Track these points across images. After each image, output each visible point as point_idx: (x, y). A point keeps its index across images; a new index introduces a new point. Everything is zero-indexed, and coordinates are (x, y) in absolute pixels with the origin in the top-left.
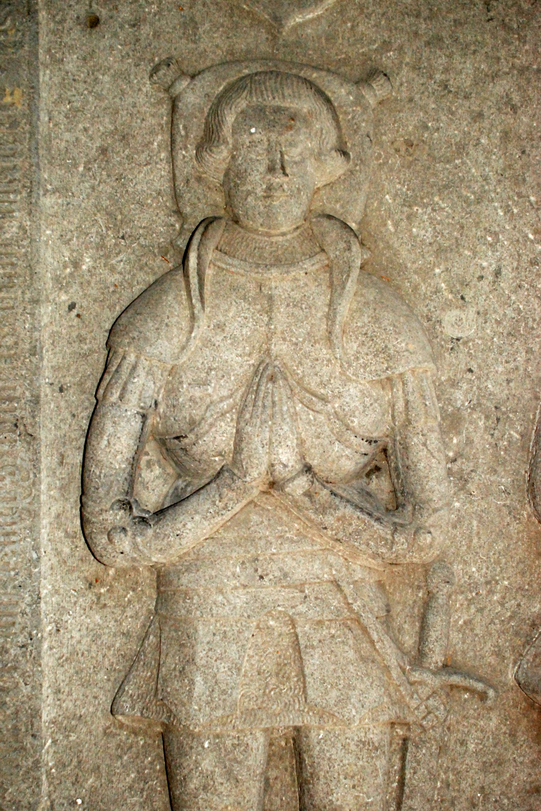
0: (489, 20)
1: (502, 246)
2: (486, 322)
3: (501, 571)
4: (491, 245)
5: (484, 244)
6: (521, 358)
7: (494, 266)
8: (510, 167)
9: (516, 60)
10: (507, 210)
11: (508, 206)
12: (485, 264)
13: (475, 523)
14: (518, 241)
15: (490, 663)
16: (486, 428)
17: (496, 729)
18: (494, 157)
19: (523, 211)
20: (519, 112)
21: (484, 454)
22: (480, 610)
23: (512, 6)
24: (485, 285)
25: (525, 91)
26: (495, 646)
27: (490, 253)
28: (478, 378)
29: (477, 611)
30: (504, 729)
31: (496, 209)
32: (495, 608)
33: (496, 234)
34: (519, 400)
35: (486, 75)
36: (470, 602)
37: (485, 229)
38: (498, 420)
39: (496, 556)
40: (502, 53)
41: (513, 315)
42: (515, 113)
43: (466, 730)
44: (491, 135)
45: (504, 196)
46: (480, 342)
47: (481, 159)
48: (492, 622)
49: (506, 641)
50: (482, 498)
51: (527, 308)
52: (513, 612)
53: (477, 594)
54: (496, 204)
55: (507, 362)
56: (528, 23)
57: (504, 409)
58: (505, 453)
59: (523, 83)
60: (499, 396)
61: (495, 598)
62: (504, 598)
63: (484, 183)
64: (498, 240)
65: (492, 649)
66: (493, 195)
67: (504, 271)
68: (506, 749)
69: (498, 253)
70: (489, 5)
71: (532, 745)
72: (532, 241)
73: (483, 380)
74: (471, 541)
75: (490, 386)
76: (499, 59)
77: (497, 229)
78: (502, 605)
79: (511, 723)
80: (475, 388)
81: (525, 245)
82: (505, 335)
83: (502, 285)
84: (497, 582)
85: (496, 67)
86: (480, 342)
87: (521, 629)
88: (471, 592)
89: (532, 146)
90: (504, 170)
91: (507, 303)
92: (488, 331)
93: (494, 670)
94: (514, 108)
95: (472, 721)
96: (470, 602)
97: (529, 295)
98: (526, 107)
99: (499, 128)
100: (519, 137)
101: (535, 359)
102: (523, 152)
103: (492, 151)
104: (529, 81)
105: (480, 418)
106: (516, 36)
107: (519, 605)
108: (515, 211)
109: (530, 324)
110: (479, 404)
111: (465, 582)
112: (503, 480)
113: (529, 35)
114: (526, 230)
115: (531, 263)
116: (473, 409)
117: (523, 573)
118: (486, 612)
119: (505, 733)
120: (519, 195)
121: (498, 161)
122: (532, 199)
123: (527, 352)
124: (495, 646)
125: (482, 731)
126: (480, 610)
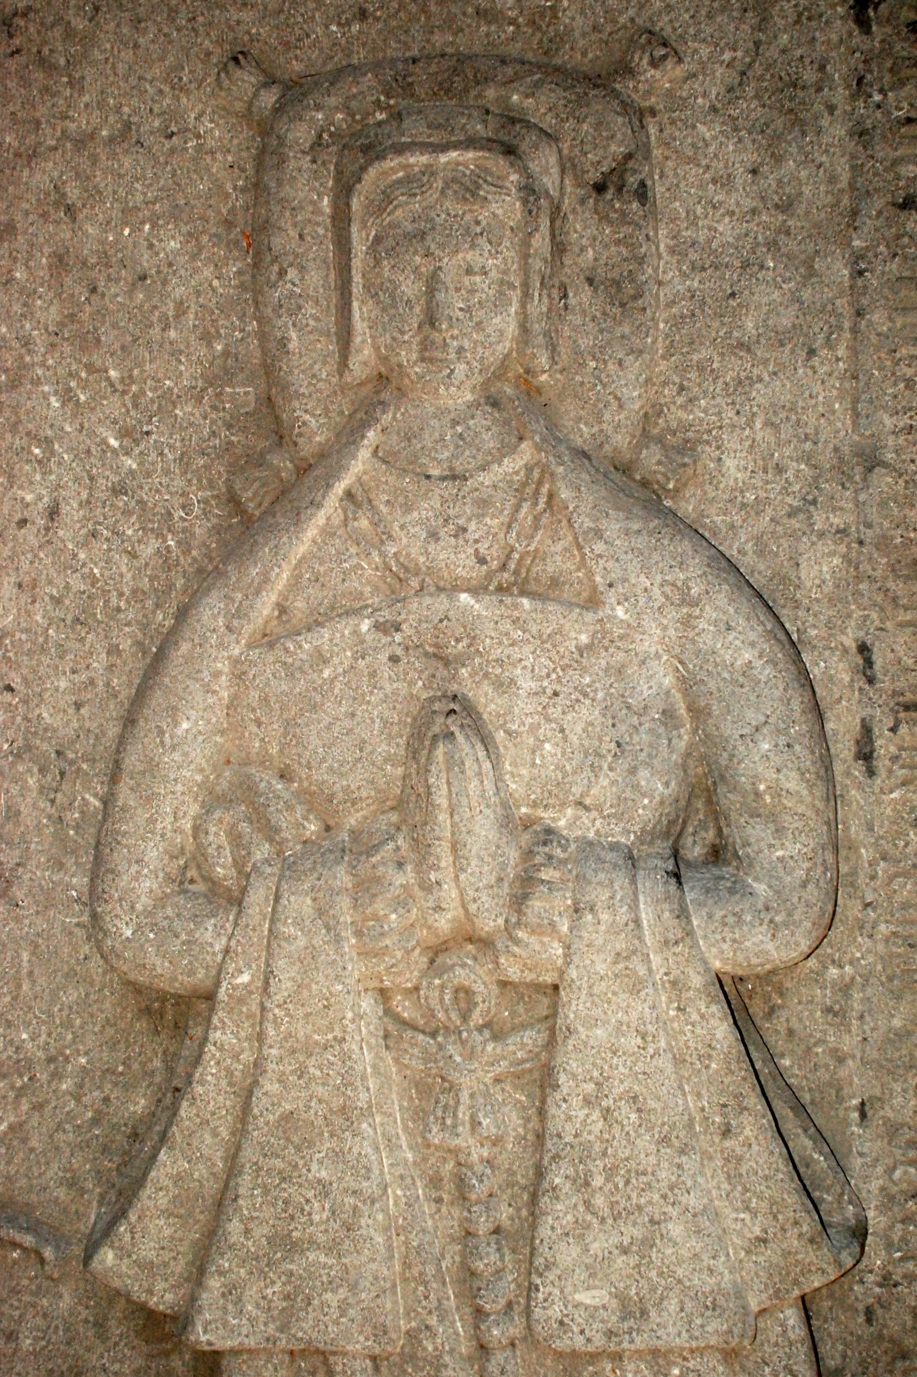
0: (12, 54)
1: (60, 463)
2: (34, 602)
3: (74, 1041)
4: (40, 462)
5: (28, 461)
6: (100, 661)
7: (46, 499)
8: (72, 317)
9: (67, 123)
10: (67, 397)
11: (70, 390)
12: (29, 498)
13: (25, 956)
14: (88, 452)
15: (57, 1198)
16: (42, 787)
17: (71, 1315)
18: (39, 302)
19: (96, 398)
20: (81, 216)
21: (40, 835)
22: (38, 1107)
23: (53, 25)
24: (30, 535)
25: (88, 178)
26: (65, 1170)
27: (38, 477)
28: (25, 702)
29: (34, 1108)
30: (85, 1313)
31: (45, 397)
32: (65, 1105)
33: (48, 441)
34: (97, 738)
35: (18, 155)
36: (21, 1092)
37: (28, 434)
38: (62, 774)
39: (65, 1013)
40: (42, 112)
41: (82, 588)
42: (74, 220)
43: (17, 1313)
44: (32, 264)
45: (61, 371)
46: (24, 637)
47: (17, 308)
48: (59, 1127)
49: (86, 1161)
50: (38, 913)
51: (107, 573)
52: (98, 1112)
53: (30, 1079)
54: (46, 388)
55: (74, 672)
56: (85, 55)
57: (71, 756)
58: (77, 833)
59: (84, 164)
60: (62, 732)
61: (64, 1087)
62: (81, 1086)
63: (23, 351)
64: (53, 453)
65: (61, 1174)
66: (40, 372)
67: (64, 509)
68: (88, 1349)
69: (53, 477)
70: (10, 26)
71: (135, 1343)
72: (114, 451)
73: (32, 705)
74: (19, 986)
75: (45, 715)
76: (38, 123)
77: (49, 433)
78: (78, 1099)
79: (98, 1304)
80: (19, 719)
81: (101, 459)
82: (68, 622)
83: (61, 533)
84: (67, 1059)
85: (31, 139)
86: (24, 637)
87: (113, 1142)
88: (21, 1076)
89: (109, 279)
90: (61, 324)
91: (70, 565)
92: (38, 618)
93: (65, 1211)
94: (70, 210)
95: (27, 1298)
96: (21, 1092)
97: (110, 550)
98: (93, 208)
99: (47, 250)
100: (84, 264)
101: (125, 663)
102: (94, 290)
103: (35, 291)
104: (94, 160)
105: (29, 771)
106: (65, 79)
107: (106, 1100)
108: (82, 398)
109: (114, 601)
110: (28, 748)
111: (9, 1057)
112: (74, 880)
113: (89, 73)
114: (103, 431)
115: (114, 490)
116: (18, 756)
117: (113, 1046)
118: (48, 1109)
119: (86, 1321)
120: (90, 368)
121: (47, 309)
122: (112, 373)
123: (108, 653)
124: (65, 1170)
125: (45, 1315)
126: (38, 1107)
